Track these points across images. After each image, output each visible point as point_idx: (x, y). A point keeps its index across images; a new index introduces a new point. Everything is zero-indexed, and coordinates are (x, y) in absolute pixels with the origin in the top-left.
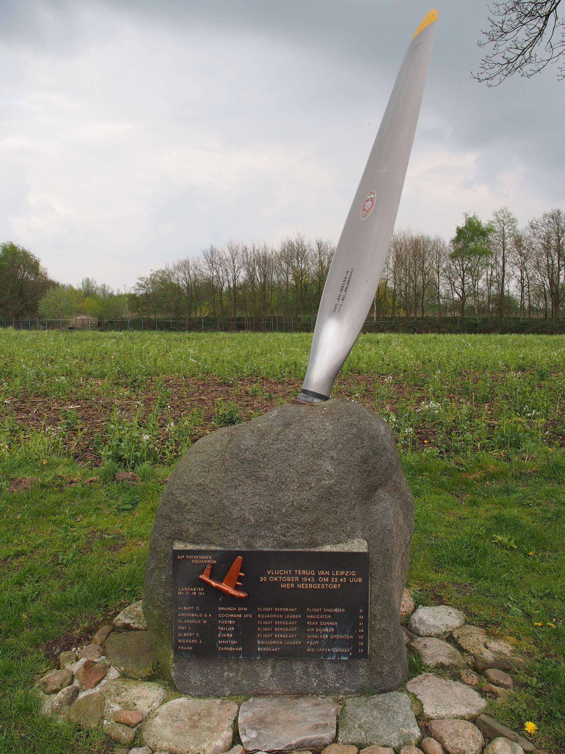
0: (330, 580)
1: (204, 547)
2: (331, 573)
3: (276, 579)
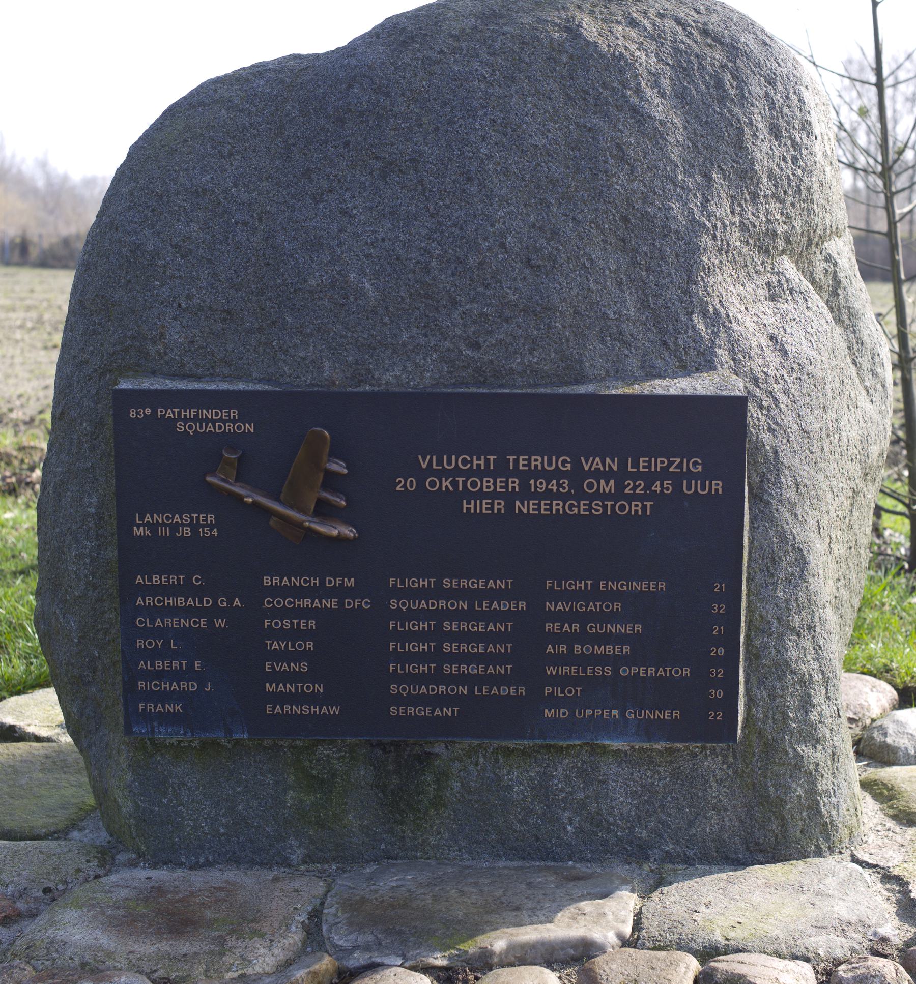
0: (620, 487)
2: (623, 465)
3: (446, 483)
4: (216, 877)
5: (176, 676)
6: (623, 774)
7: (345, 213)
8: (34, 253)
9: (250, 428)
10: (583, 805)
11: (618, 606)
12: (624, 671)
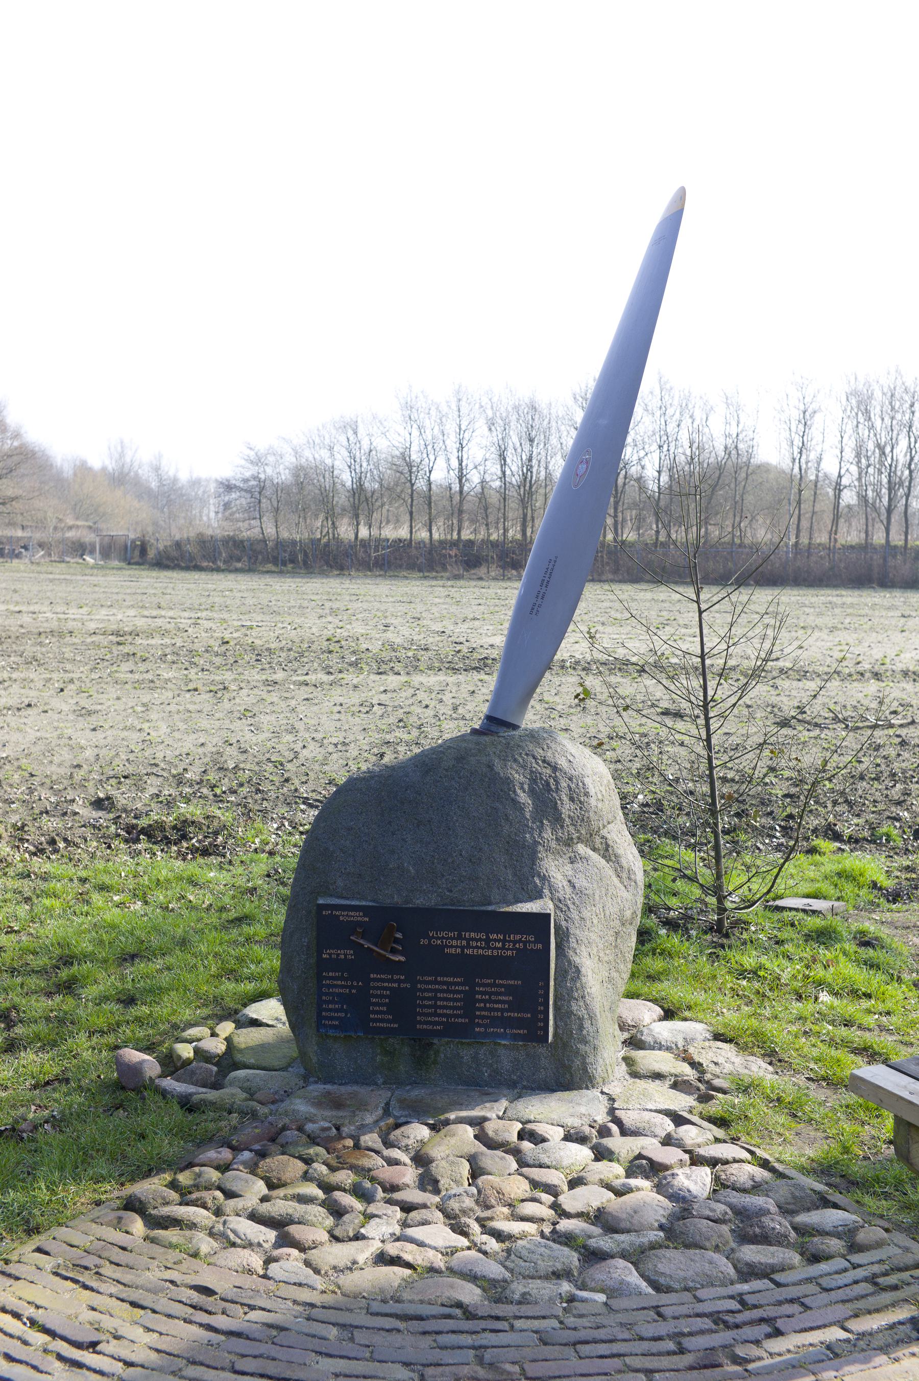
0: (504, 945)
4: (350, 1089)
5: (336, 1011)
6: (506, 1054)
8: (151, 554)
10: (491, 1065)
12: (505, 1014)
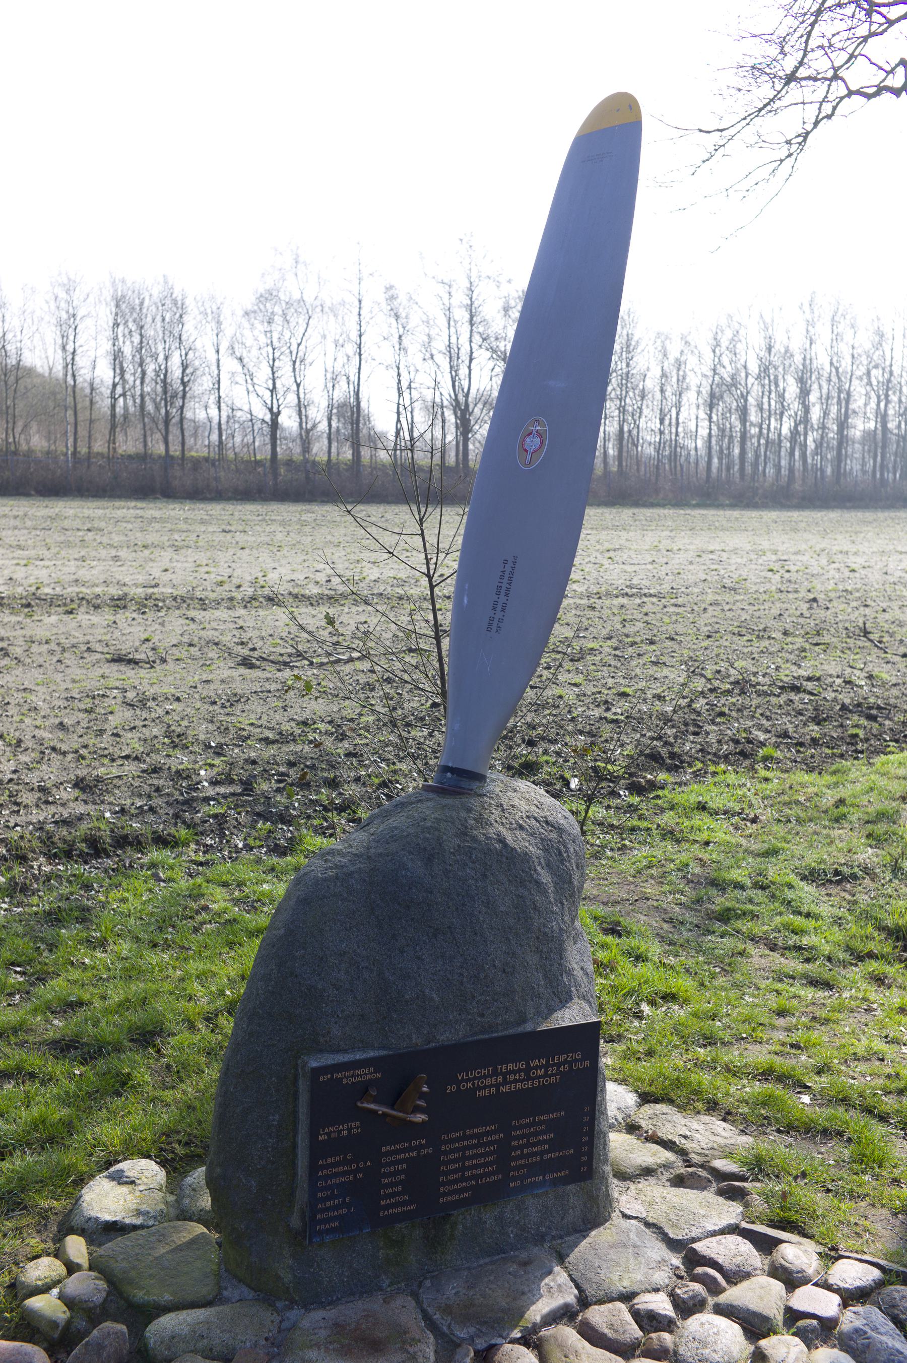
0: (546, 1071)
1: (358, 1056)
2: (548, 1061)
3: (470, 1085)
5: (336, 1208)
7: (418, 958)
9: (379, 1075)
10: (518, 1222)
11: (543, 1127)
